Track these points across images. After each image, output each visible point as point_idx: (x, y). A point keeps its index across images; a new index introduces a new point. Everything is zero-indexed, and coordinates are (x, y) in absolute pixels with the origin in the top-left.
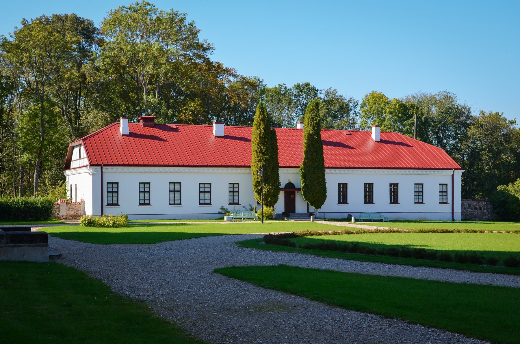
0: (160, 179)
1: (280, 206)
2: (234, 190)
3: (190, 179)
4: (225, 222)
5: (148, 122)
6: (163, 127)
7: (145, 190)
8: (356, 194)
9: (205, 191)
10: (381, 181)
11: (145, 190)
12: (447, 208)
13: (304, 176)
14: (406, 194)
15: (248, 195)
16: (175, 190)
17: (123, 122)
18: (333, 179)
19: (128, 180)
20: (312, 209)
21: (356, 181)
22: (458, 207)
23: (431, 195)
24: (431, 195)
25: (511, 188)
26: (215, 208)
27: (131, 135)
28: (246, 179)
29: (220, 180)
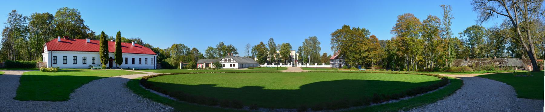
0: (70, 56)
1: (108, 65)
2: (94, 59)
3: (80, 56)
4: (92, 70)
5: (67, 38)
6: (71, 39)
7: (65, 59)
8: (130, 61)
9: (85, 59)
10: (137, 57)
11: (65, 59)
12: (153, 65)
13: (116, 55)
14: (143, 61)
15: (98, 60)
16: (75, 59)
17: (59, 38)
18: (124, 56)
19: (60, 55)
20: (118, 65)
21: (130, 57)
22: (156, 65)
23: (149, 62)
24: (149, 62)
25: (166, 60)
26: (87, 65)
27: (61, 41)
28: (98, 56)
29: (89, 56)
